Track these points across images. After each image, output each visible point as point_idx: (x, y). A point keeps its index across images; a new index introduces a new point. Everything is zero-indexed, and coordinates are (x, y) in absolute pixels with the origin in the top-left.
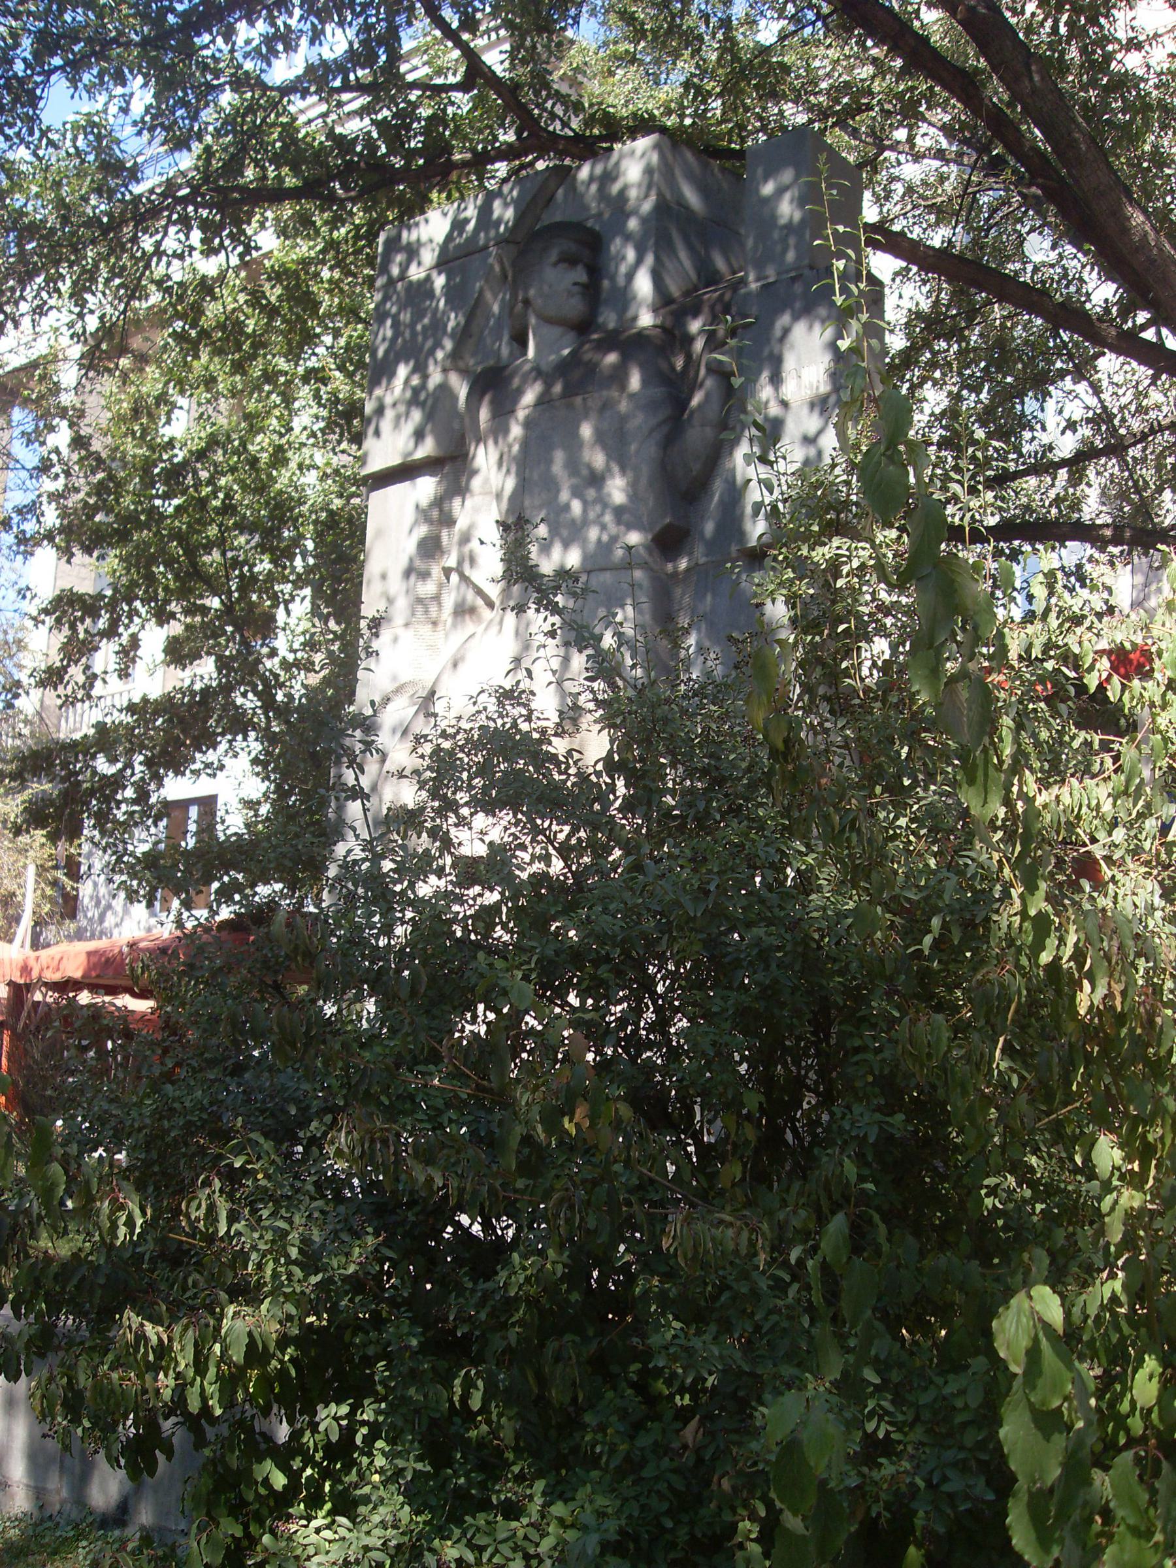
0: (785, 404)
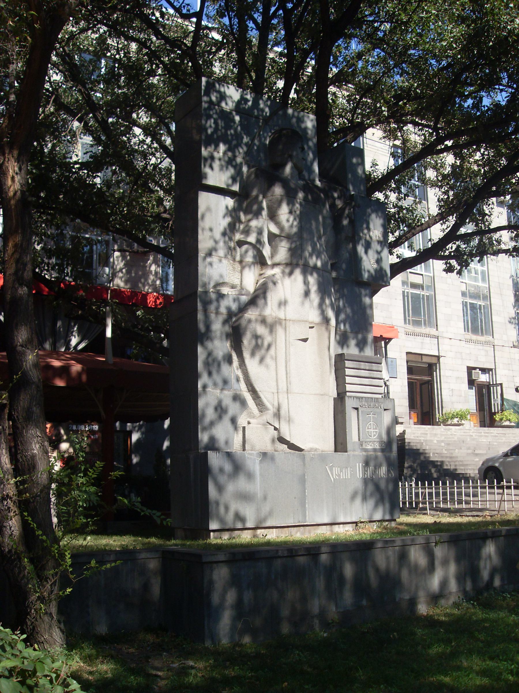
0: (371, 238)
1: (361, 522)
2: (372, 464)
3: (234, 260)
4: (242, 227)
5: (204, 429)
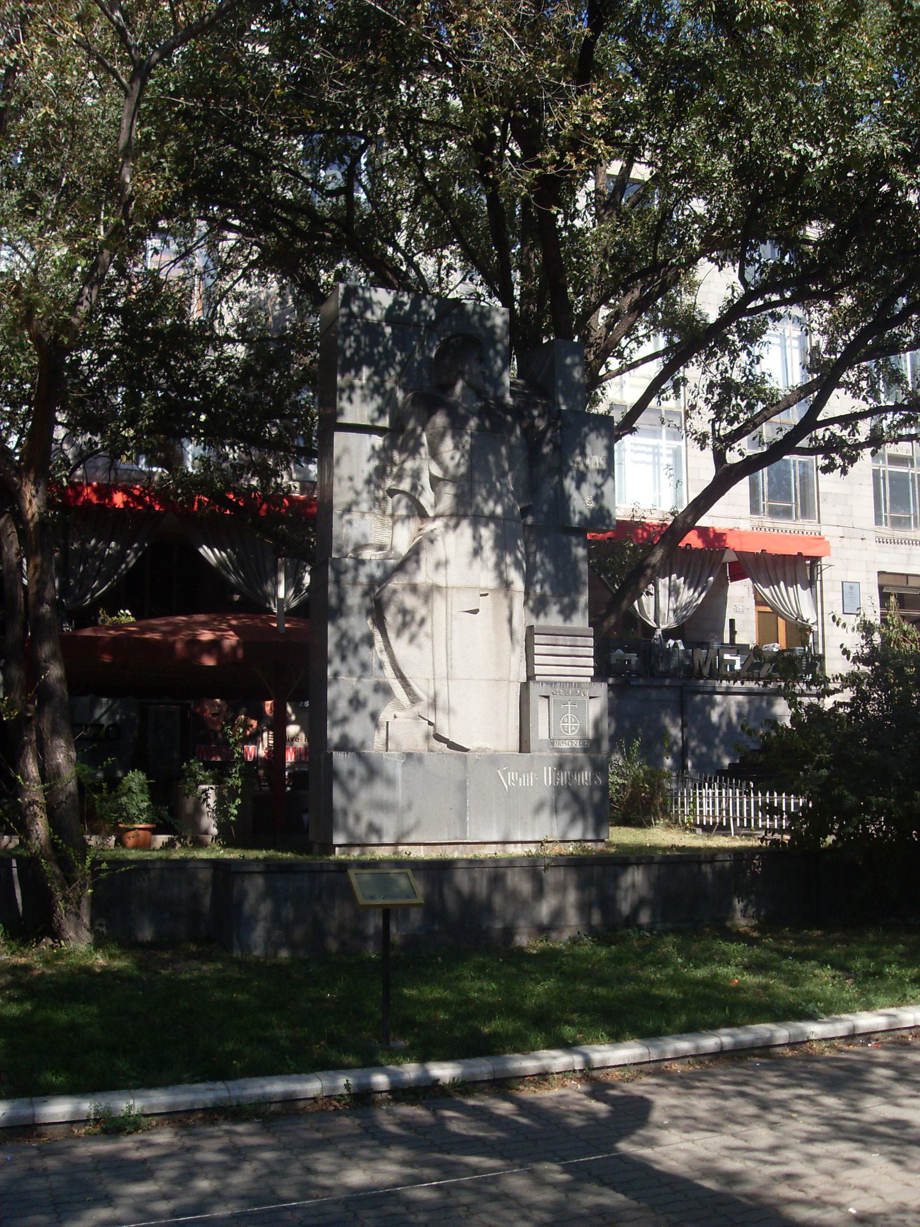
0: (586, 467)
1: (547, 842)
2: (568, 767)
3: (384, 512)
4: (395, 470)
5: (335, 723)
